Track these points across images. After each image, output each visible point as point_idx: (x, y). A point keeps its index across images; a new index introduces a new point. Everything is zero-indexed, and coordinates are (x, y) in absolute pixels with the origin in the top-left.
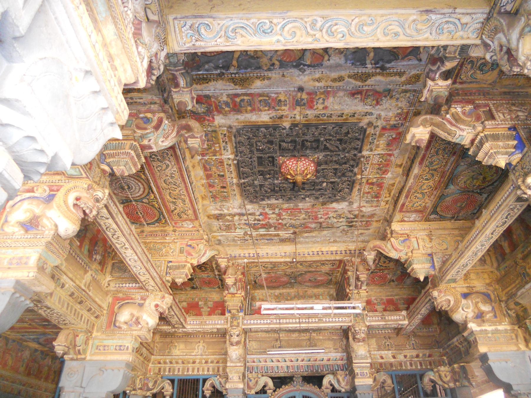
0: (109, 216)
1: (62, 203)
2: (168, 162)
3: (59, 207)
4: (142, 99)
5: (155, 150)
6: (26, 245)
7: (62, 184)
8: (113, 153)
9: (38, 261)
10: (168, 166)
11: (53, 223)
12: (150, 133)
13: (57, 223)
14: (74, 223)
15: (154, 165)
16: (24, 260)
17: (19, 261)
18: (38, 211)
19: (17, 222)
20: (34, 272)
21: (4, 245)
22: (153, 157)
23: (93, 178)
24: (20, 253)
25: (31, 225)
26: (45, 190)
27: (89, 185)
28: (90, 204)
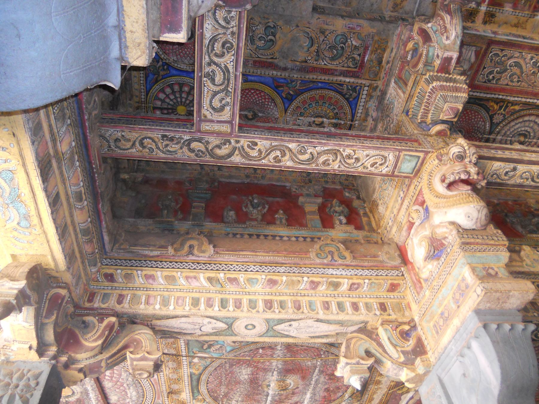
0: (512, 165)
1: (437, 200)
2: (511, 61)
3: (437, 206)
4: (392, 49)
5: (455, 55)
6: (448, 269)
7: (419, 187)
8: (424, 109)
9: (474, 273)
10: (517, 64)
11: (447, 224)
12: (428, 52)
13: (452, 220)
14: (468, 202)
15: (506, 82)
16: (463, 285)
17: (460, 292)
18: (427, 232)
19: (425, 260)
20: (478, 286)
21: (436, 291)
22: (491, 77)
23: (433, 147)
24: (452, 283)
25: (436, 248)
26: (417, 210)
27: (437, 157)
28: (457, 169)
